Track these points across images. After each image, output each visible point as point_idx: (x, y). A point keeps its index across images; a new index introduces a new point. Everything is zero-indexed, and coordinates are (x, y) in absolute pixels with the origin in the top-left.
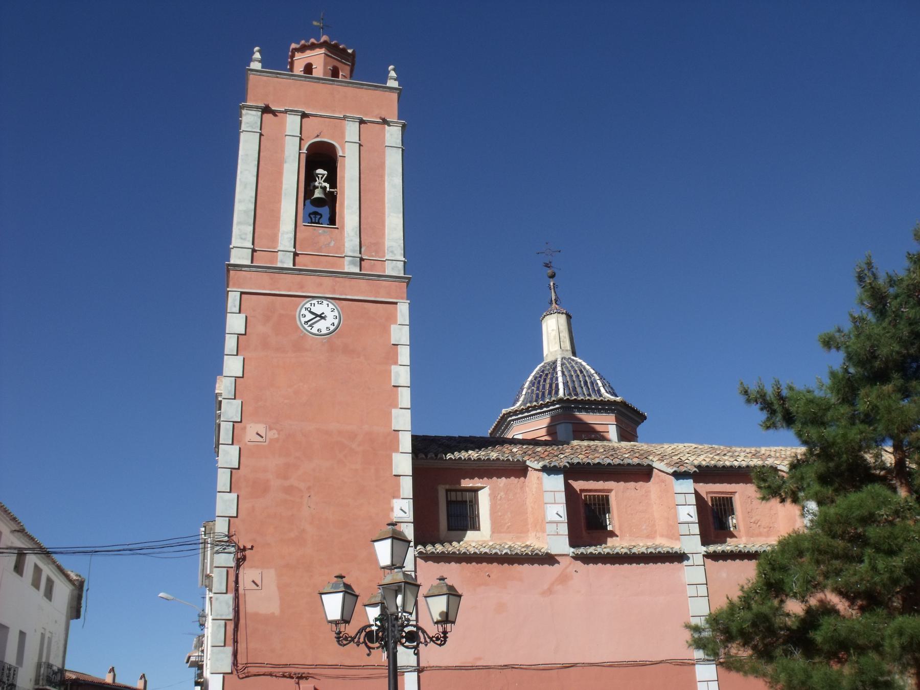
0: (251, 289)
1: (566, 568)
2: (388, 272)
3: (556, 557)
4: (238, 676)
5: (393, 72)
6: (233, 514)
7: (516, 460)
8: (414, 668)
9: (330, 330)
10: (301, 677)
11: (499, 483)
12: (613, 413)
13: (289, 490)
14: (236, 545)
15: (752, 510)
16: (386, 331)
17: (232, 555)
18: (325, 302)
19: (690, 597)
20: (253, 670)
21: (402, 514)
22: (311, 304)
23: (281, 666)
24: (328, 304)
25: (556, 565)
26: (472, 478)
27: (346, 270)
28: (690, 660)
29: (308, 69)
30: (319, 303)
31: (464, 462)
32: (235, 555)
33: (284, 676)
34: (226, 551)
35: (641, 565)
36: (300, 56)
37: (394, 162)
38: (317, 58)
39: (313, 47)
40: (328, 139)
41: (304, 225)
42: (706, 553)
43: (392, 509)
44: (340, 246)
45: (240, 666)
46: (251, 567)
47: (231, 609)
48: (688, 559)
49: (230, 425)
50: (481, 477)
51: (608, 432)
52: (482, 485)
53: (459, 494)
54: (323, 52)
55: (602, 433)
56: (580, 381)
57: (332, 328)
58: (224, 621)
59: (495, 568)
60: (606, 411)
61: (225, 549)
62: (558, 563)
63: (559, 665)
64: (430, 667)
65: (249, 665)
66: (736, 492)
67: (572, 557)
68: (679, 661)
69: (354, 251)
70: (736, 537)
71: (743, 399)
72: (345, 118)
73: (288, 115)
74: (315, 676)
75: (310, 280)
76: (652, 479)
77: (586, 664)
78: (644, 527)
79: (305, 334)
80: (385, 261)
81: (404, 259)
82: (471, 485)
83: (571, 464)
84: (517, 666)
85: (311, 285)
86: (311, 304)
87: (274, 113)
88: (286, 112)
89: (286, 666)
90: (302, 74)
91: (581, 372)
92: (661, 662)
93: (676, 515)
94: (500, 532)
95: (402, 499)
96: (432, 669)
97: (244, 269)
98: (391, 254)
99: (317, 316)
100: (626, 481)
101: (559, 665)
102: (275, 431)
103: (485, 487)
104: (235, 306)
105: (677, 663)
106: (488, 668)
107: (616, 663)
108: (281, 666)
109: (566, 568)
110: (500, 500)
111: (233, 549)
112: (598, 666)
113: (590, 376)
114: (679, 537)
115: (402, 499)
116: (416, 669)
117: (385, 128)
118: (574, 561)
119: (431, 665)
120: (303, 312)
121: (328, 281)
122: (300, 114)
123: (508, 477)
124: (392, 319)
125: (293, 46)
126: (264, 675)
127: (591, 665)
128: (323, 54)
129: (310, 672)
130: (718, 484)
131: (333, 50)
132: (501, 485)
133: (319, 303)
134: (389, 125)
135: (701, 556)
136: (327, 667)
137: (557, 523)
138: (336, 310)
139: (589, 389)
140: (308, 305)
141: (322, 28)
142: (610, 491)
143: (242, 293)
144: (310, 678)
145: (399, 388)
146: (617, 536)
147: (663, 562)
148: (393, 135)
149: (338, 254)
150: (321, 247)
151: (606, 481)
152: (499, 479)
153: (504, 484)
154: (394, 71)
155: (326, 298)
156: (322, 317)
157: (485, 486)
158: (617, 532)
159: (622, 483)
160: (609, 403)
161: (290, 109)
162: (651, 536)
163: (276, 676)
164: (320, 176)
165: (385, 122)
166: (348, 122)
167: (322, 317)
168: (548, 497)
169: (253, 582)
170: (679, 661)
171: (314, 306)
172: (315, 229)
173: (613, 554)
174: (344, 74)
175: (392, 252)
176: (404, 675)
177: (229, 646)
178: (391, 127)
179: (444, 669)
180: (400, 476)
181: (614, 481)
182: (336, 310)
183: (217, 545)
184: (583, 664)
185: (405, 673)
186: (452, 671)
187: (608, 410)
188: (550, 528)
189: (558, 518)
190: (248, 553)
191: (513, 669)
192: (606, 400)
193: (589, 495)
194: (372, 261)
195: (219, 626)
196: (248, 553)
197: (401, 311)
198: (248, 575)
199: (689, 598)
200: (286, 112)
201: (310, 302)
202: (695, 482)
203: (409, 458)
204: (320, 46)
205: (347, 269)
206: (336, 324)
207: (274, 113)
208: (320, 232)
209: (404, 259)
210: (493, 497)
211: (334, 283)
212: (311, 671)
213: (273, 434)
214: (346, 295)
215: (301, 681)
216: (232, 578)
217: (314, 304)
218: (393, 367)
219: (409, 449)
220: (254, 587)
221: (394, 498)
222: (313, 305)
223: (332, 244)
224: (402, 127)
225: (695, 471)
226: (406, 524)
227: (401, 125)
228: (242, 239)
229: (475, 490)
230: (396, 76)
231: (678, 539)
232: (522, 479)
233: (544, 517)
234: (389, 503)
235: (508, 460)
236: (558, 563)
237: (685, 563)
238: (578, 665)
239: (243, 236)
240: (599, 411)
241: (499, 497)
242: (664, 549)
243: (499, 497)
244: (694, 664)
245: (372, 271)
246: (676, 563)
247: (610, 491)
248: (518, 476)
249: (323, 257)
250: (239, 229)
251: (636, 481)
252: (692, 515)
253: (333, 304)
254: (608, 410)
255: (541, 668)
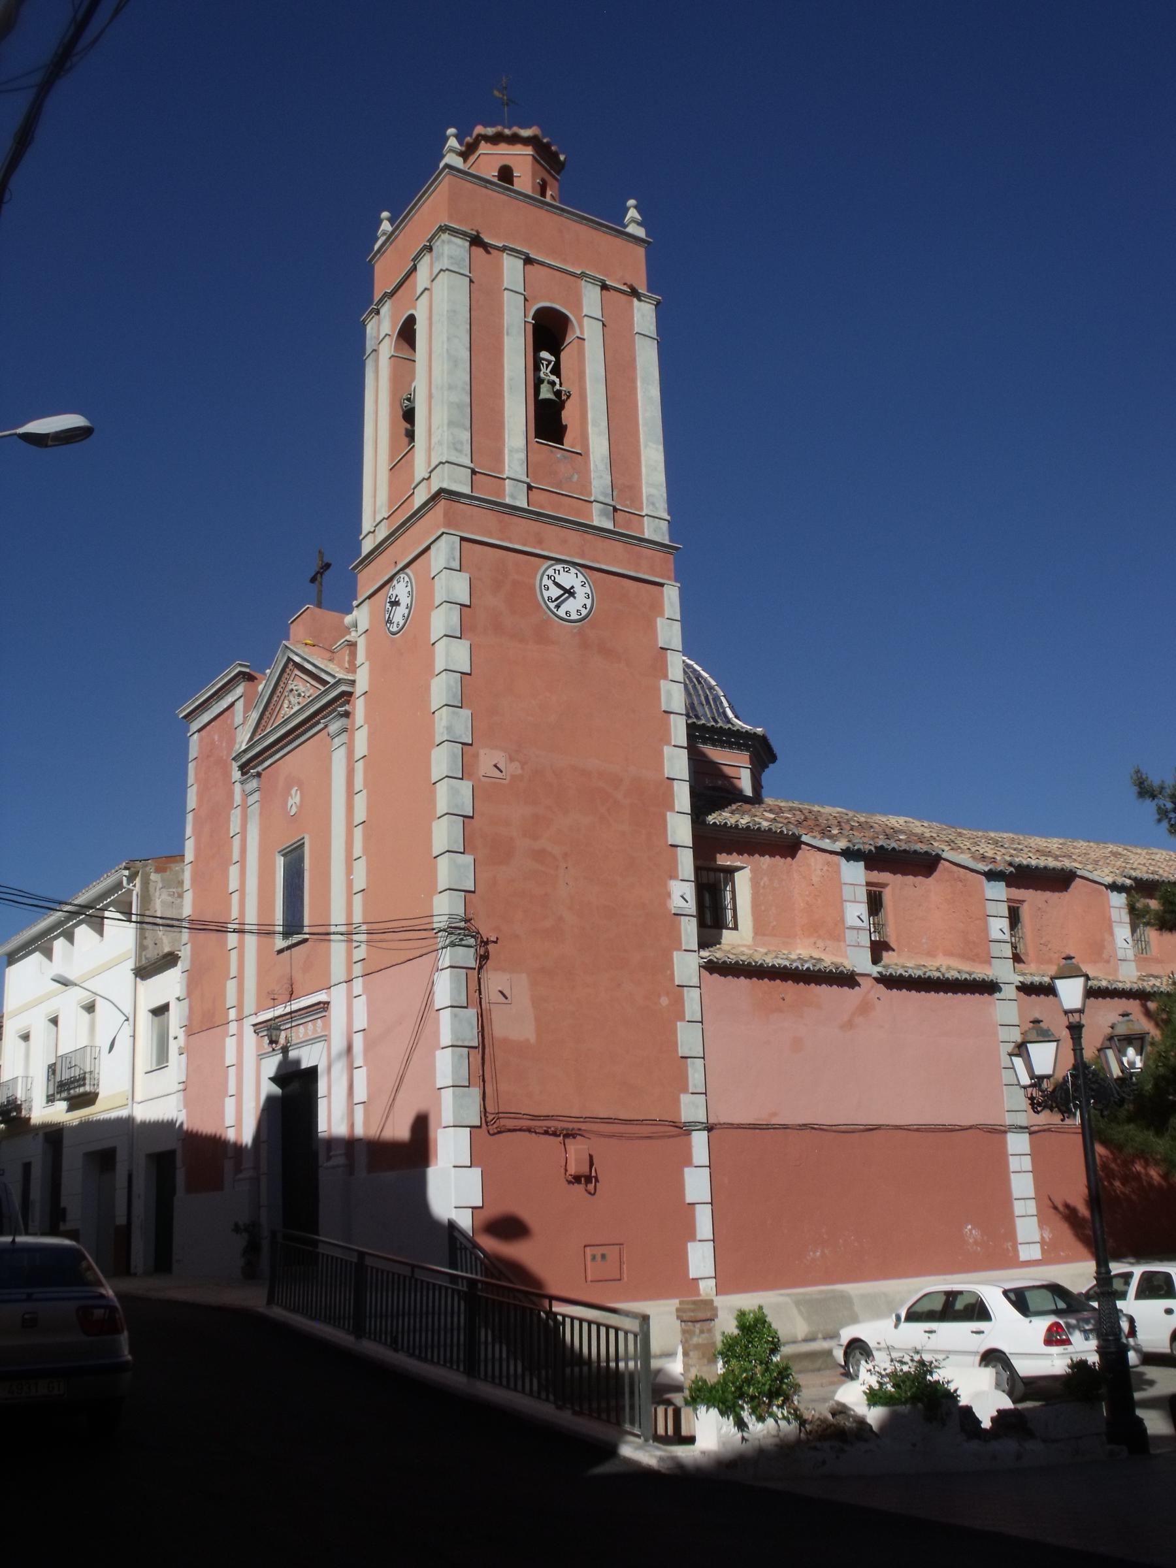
0: (473, 533)
1: (869, 992)
2: (647, 535)
3: (856, 977)
4: (488, 1132)
5: (454, 139)
6: (470, 887)
7: (791, 833)
8: (704, 1125)
9: (581, 614)
10: (569, 1135)
11: (761, 864)
12: (747, 751)
13: (540, 855)
14: (476, 935)
15: (1042, 926)
16: (651, 628)
17: (473, 950)
18: (573, 570)
19: (1002, 1042)
20: (510, 1123)
21: (682, 903)
22: (555, 570)
23: (542, 1118)
24: (577, 574)
25: (857, 988)
26: (729, 853)
27: (596, 523)
28: (1001, 1126)
29: (506, 174)
30: (566, 570)
31: (735, 831)
32: (476, 950)
33: (546, 1133)
34: (463, 943)
35: (949, 994)
36: (490, 149)
37: (647, 358)
38: (521, 158)
39: (515, 139)
40: (561, 306)
41: (537, 442)
42: (1020, 984)
43: (669, 895)
44: (585, 485)
45: (490, 1117)
46: (496, 970)
47: (475, 1031)
48: (1000, 990)
49: (458, 748)
50: (740, 853)
51: (740, 778)
52: (742, 865)
53: (712, 874)
54: (531, 153)
55: (732, 779)
56: (699, 695)
57: (584, 612)
58: (466, 1049)
59: (789, 988)
60: (739, 747)
61: (461, 940)
62: (859, 985)
63: (861, 1127)
64: (720, 1124)
65: (501, 1115)
66: (1024, 901)
67: (876, 979)
68: (990, 1127)
69: (606, 495)
70: (1024, 963)
71: (1135, 789)
72: (583, 275)
73: (583, 282)
74: (585, 1134)
75: (550, 531)
76: (935, 874)
77: (892, 1126)
78: (924, 940)
79: (549, 616)
80: (592, 502)
81: (668, 518)
82: (728, 863)
83: (881, 848)
84: (816, 1126)
85: (553, 541)
86: (555, 570)
87: (486, 247)
88: (504, 249)
89: (547, 1117)
90: (495, 180)
91: (700, 682)
92: (971, 1127)
93: (986, 929)
94: (764, 935)
95: (681, 880)
96: (723, 1126)
97: (463, 500)
98: (651, 507)
99: (566, 591)
100: (904, 874)
101: (861, 1127)
102: (517, 764)
103: (746, 867)
104: (454, 559)
105: (988, 1130)
106: (785, 1127)
107: (924, 1127)
108: (542, 1118)
109: (869, 992)
110: (764, 887)
111: (472, 941)
112: (905, 1129)
113: (711, 688)
114: (988, 959)
115: (681, 880)
116: (705, 1127)
117: (632, 302)
118: (876, 984)
119: (722, 1122)
120: (545, 581)
121: (574, 537)
122: (523, 257)
123: (772, 855)
124: (656, 608)
125: (479, 130)
126: (520, 1130)
127: (896, 1127)
128: (531, 157)
129: (583, 1128)
130: (1014, 889)
131: (544, 154)
132: (765, 867)
133: (566, 570)
134: (640, 300)
135: (1013, 988)
136: (599, 1120)
137: (858, 929)
138: (587, 585)
139: (712, 709)
140: (550, 572)
141: (507, 104)
142: (884, 885)
143: (463, 539)
144: (578, 1136)
145: (672, 715)
146: (893, 950)
147: (1104, 997)
148: (644, 315)
149: (583, 496)
150: (561, 481)
151: (881, 871)
152: (762, 857)
153: (769, 866)
154: (456, 138)
155: (574, 564)
156: (570, 593)
157: (745, 865)
158: (893, 945)
159: (899, 876)
160: (739, 734)
161: (511, 246)
162: (931, 954)
163: (536, 1133)
164: (545, 363)
165: (634, 293)
166: (586, 283)
167: (570, 593)
168: (847, 892)
169: (501, 992)
170: (990, 1127)
171: (559, 574)
172: (552, 452)
173: (925, 978)
174: (553, 194)
175: (653, 504)
176: (690, 1134)
177: (474, 1086)
178: (642, 303)
179: (736, 1128)
180: (677, 846)
181: (890, 872)
182: (587, 585)
183: (452, 934)
184: (888, 1125)
185: (694, 1133)
186: (745, 1130)
187: (741, 745)
188: (850, 936)
189: (1126, 945)
190: (491, 947)
191: (813, 1131)
192: (735, 729)
193: (874, 891)
194: (627, 514)
195: (461, 1056)
196: (491, 947)
197: (669, 599)
198: (495, 981)
199: (1002, 1044)
200: (504, 249)
201: (554, 567)
202: (1008, 886)
203: (687, 820)
204: (526, 141)
205: (597, 522)
206: (588, 606)
207: (486, 247)
208: (559, 456)
209: (668, 518)
210: (755, 882)
211: (583, 542)
212: (583, 1126)
213: (514, 768)
214: (598, 562)
215: (567, 1141)
216: (473, 985)
217: (559, 571)
218: (662, 682)
219: (688, 809)
220: (502, 999)
221: (671, 879)
222: (557, 572)
223: (575, 478)
224: (656, 306)
225: (1011, 872)
226: (688, 918)
227: (655, 303)
228: (456, 449)
229: (731, 871)
230: (639, 218)
231: (990, 963)
232: (789, 859)
233: (843, 920)
234: (665, 885)
235: (782, 832)
236: (859, 985)
237: (997, 995)
238: (882, 1127)
239: (459, 447)
240: (730, 745)
241: (762, 884)
242: (979, 976)
243: (762, 884)
244: (1005, 1132)
245: (627, 530)
246: (824, 985)
247: (884, 885)
248: (783, 856)
249: (564, 497)
250: (452, 434)
251: (915, 875)
252: (1005, 932)
253: (584, 576)
254: (741, 745)
255: (843, 1130)
